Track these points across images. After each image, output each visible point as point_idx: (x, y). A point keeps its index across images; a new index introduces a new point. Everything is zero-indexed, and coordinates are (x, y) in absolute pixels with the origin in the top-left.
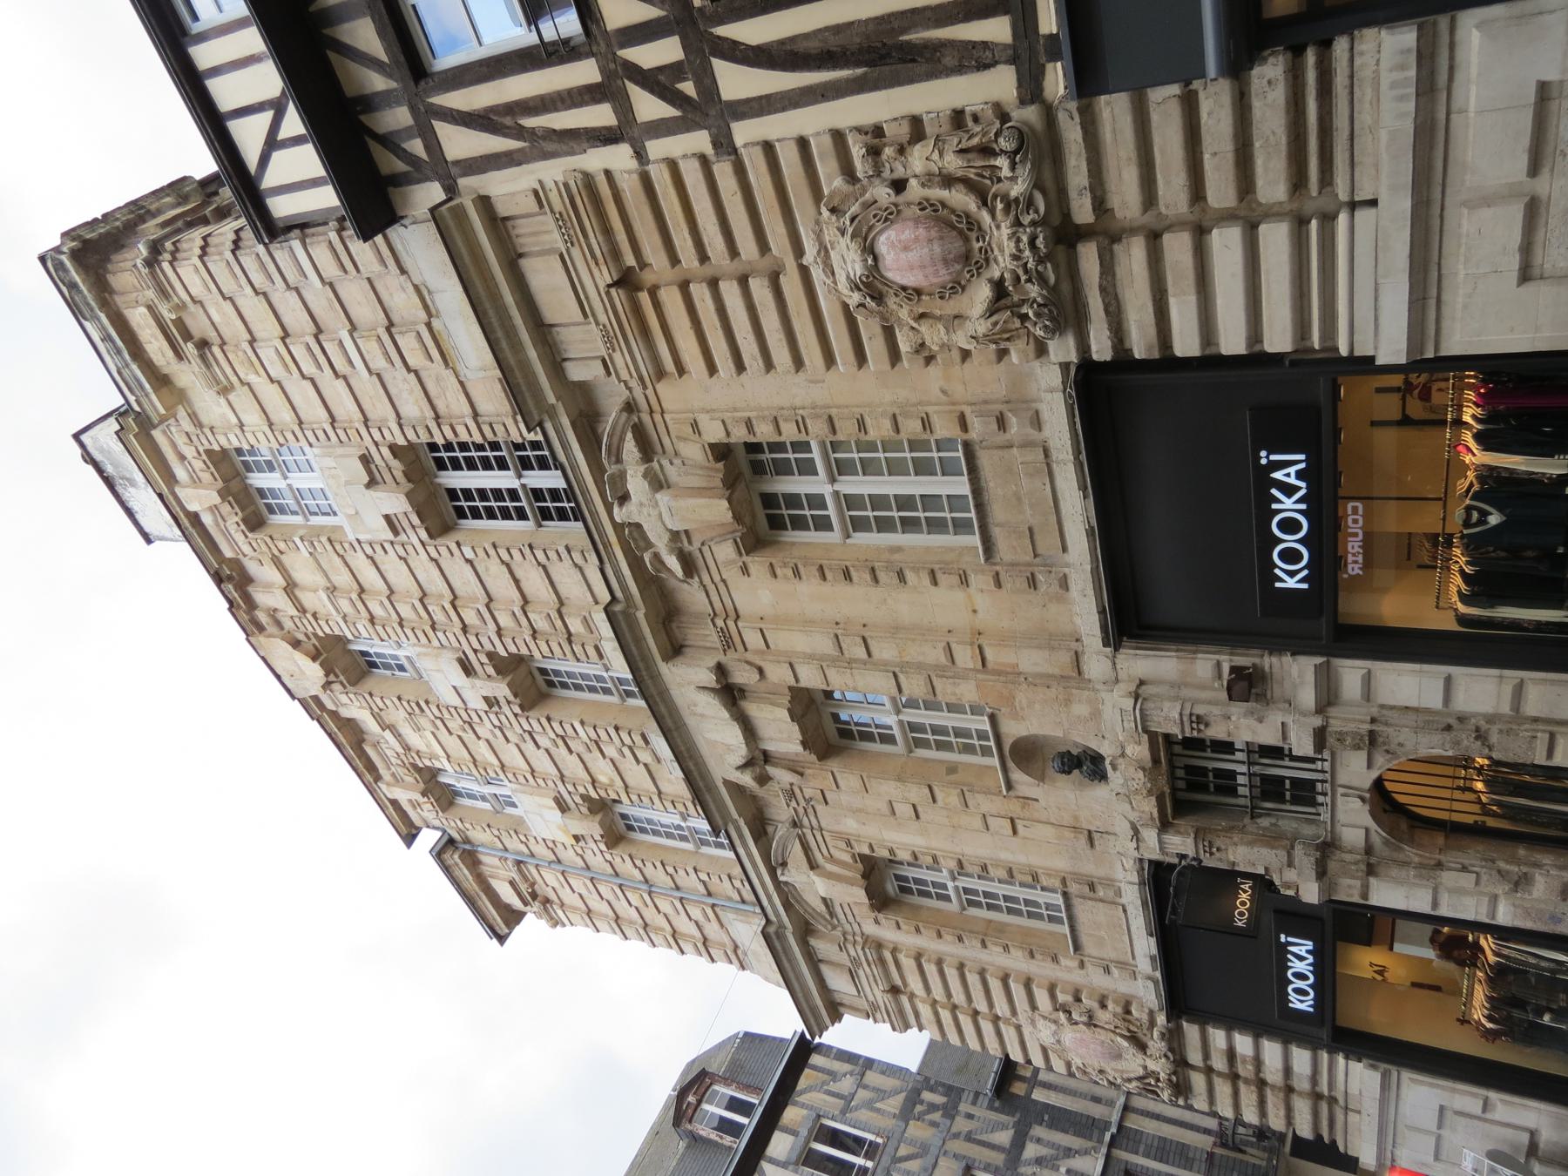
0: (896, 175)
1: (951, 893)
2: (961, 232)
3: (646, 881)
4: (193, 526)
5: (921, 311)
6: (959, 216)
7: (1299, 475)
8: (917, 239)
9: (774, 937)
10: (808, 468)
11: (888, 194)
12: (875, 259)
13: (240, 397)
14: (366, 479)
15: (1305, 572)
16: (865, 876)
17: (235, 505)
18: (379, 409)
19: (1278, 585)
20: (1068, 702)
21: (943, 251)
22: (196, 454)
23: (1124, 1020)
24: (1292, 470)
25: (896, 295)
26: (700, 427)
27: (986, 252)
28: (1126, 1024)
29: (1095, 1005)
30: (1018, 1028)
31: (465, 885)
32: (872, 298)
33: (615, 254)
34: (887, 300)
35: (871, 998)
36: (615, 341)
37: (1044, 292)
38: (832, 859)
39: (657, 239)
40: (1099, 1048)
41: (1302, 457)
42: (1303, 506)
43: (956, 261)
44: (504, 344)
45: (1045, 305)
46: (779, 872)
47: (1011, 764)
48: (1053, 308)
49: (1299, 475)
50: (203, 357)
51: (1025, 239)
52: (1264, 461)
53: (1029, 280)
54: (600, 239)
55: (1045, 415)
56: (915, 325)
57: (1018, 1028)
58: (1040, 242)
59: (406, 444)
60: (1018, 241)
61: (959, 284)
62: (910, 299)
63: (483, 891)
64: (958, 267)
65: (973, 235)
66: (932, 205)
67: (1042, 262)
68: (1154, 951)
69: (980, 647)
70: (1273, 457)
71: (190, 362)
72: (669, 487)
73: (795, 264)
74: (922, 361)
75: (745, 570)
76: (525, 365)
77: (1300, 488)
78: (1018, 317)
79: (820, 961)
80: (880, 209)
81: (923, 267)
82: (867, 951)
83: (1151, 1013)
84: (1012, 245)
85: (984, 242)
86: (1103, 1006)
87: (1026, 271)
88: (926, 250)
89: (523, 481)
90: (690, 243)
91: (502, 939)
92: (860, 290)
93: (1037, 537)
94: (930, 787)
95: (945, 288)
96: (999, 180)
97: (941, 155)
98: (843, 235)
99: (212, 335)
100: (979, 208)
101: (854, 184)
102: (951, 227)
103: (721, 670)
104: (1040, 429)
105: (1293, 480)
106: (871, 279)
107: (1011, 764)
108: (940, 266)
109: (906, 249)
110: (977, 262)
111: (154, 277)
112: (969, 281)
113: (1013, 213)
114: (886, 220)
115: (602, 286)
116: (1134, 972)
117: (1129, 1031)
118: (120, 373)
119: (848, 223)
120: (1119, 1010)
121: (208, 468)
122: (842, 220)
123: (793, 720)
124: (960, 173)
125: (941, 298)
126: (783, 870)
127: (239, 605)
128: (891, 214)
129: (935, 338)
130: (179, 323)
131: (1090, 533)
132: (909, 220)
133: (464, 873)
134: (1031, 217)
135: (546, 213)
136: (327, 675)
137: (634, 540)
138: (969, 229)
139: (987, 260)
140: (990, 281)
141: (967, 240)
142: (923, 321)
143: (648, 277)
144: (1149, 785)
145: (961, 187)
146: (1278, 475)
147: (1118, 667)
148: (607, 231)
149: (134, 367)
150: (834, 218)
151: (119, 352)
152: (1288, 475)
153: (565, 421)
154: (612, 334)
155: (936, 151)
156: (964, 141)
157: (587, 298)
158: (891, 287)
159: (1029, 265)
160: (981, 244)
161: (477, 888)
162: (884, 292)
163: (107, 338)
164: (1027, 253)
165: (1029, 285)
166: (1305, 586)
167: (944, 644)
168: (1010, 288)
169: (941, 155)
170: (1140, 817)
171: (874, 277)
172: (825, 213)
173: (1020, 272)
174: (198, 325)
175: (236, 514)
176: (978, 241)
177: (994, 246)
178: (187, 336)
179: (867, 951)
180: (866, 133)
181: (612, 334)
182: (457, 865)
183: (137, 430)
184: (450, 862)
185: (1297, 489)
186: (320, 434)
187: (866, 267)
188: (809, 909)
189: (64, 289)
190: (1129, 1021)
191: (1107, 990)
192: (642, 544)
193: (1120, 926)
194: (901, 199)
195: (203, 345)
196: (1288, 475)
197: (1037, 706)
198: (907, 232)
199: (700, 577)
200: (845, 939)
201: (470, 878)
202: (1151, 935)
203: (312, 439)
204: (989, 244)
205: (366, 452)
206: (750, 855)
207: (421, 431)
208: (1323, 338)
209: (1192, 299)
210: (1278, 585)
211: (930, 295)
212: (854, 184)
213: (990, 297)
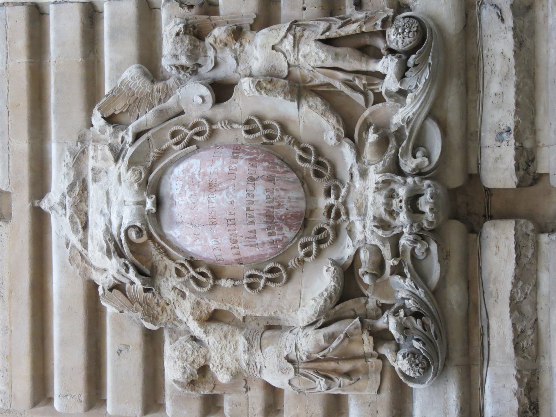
0: (220, 74)
2: (303, 180)
5: (214, 305)
8: (231, 175)
11: (202, 97)
12: (159, 203)
21: (269, 200)
25: (179, 273)
27: (338, 215)
32: (140, 272)
37: (420, 292)
43: (286, 220)
45: (417, 315)
48: (429, 322)
51: (402, 192)
53: (398, 270)
60: (391, 195)
61: (286, 266)
62: (199, 283)
64: (289, 234)
65: (320, 185)
66: (265, 127)
67: (423, 238)
78: (371, 333)
80: (185, 126)
81: (231, 222)
84: (381, 199)
85: (337, 198)
87: (396, 253)
88: (242, 194)
92: (121, 255)
95: (261, 271)
96: (379, 98)
97: (296, 43)
98: (116, 160)
100: (339, 139)
101: (153, 82)
102: (289, 165)
106: (145, 238)
108: (260, 226)
109: (211, 187)
110: (320, 231)
112: (302, 262)
113: (391, 152)
114: (191, 142)
119: (129, 139)
122: (121, 134)
124: (320, 78)
125: (251, 286)
128: (198, 134)
129: (228, 359)
132: (227, 146)
134: (418, 160)
138: (318, 174)
139: (337, 229)
140: (335, 263)
141: (310, 193)
142: (213, 326)
145: (317, 102)
150: (109, 129)
155: (290, 37)
156: (334, 28)
160: (332, 200)
162: (161, 268)
165: (397, 279)
168: (367, 279)
169: (296, 43)
171: (151, 237)
172: (98, 120)
173: (387, 252)
177: (352, 206)
180: (191, 7)
194: (220, 112)
204: (345, 203)
211: (235, 280)
212: (153, 82)
213: (331, 289)
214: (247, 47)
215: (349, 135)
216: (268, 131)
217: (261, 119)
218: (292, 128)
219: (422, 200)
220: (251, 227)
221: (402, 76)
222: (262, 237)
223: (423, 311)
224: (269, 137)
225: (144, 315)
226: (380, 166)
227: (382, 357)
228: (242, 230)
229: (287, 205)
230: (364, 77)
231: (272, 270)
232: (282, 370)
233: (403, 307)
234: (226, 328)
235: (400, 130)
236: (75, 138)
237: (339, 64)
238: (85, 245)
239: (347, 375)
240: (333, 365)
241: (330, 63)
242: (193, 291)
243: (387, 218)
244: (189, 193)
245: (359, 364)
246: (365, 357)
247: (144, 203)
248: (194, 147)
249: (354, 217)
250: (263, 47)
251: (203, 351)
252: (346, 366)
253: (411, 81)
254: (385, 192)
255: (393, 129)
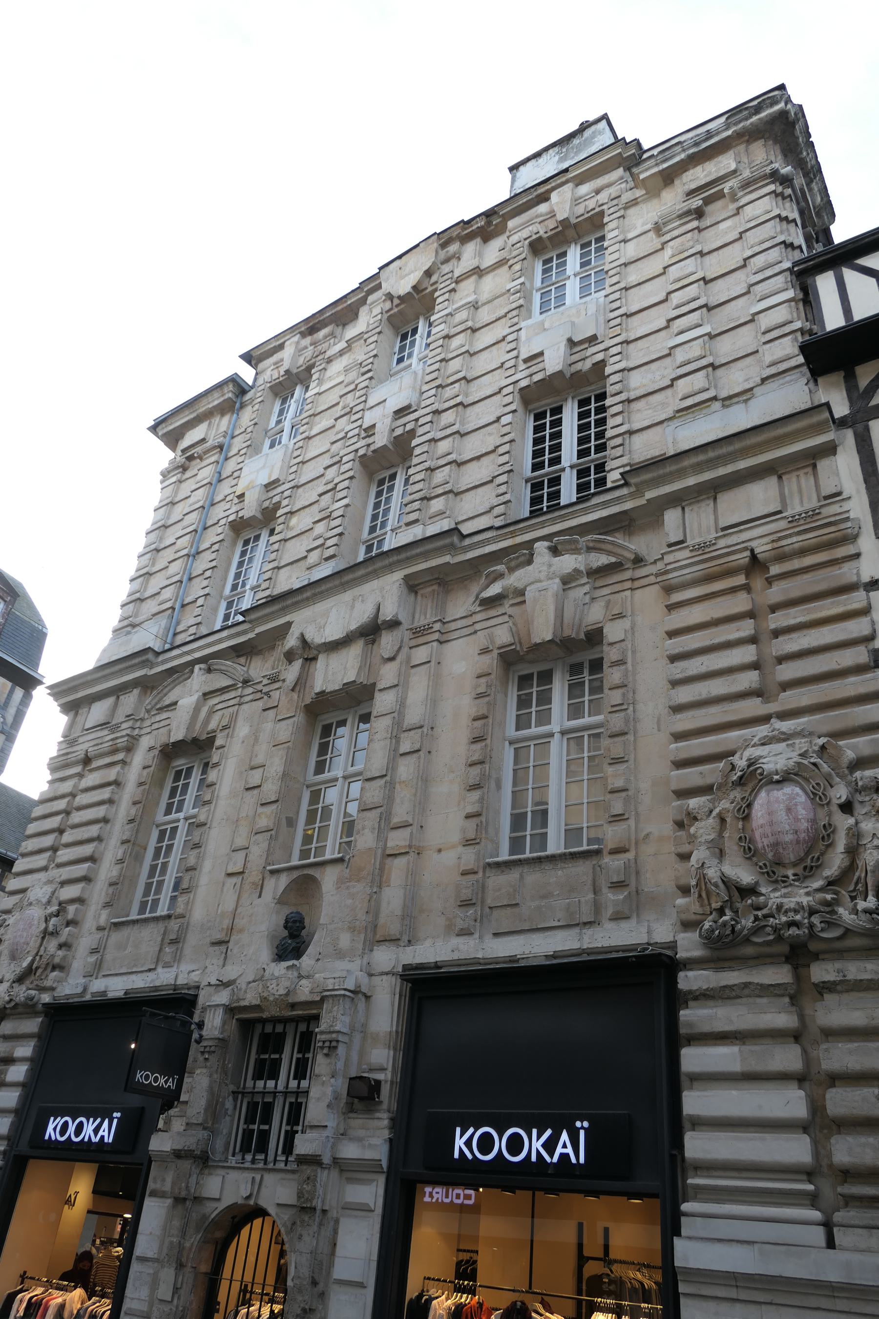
0: (857, 806)
1: (173, 816)
2: (802, 860)
3: (198, 553)
4: (538, 196)
5: (728, 820)
6: (818, 859)
7: (564, 1157)
8: (797, 820)
9: (144, 658)
10: (575, 711)
11: (840, 797)
12: (778, 782)
13: (652, 242)
14: (576, 339)
15: (470, 1156)
16: (195, 740)
17: (553, 232)
18: (637, 354)
19: (458, 1130)
20: (352, 929)
22: (600, 202)
23: (48, 964)
24: (569, 1150)
25: (743, 799)
26: (618, 621)
27: (784, 882)
28: (43, 966)
29: (62, 939)
30: (45, 869)
31: (204, 401)
32: (741, 778)
33: (782, 557)
34: (739, 789)
35: (81, 740)
36: (700, 552)
37: (745, 932)
38: (212, 712)
39: (796, 593)
40: (22, 941)
41: (582, 1160)
42: (534, 1158)
44: (701, 457)
45: (733, 931)
46: (203, 666)
47: (295, 874)
48: (730, 938)
49: (564, 1157)
50: (688, 212)
51: (798, 917)
52: (578, 1124)
53: (756, 918)
54: (796, 546)
55: (624, 924)
56: (714, 813)
57: (45, 869)
58: (793, 931)
59: (606, 374)
60: (796, 911)
61: (753, 856)
63: (198, 416)
65: (799, 870)
66: (828, 835)
67: (775, 931)
68: (111, 995)
69: (407, 853)
70: (582, 1133)
71: (684, 202)
72: (564, 590)
73: (772, 711)
74: (679, 818)
75: (485, 651)
76: (681, 474)
77: (552, 1156)
79: (118, 697)
80: (824, 789)
81: (771, 823)
82: (126, 739)
83: (53, 989)
84: (792, 905)
86: (61, 946)
87: (765, 916)
88: (787, 827)
89: (568, 470)
90: (792, 622)
91: (154, 429)
92: (749, 766)
93: (509, 910)
94: (276, 801)
96: (853, 898)
99: (707, 222)
100: (826, 878)
103: (394, 624)
104: (610, 919)
105: (559, 1150)
106: (760, 778)
107: (295, 874)
108: (772, 839)
109: (789, 810)
111: (760, 178)
115: (753, 544)
116: (91, 976)
117: (37, 968)
118: (769, 98)
119: (812, 760)
120: (57, 960)
121: (588, 212)
122: (815, 755)
123: (344, 685)
126: (204, 669)
127: (466, 229)
129: (701, 831)
130: (720, 195)
131: (513, 959)
133: (216, 400)
134: (819, 925)
135: (819, 501)
136: (399, 297)
137: (518, 557)
138: (805, 868)
139: (776, 882)
143: (758, 583)
144: (271, 999)
145: (847, 863)
146: (565, 1137)
147: (384, 977)
148: (803, 552)
149: (683, 156)
150: (816, 748)
151: (696, 144)
152: (564, 1146)
153: (628, 506)
154: (707, 550)
157: (741, 531)
158: (750, 795)
159: (771, 919)
160: (792, 877)
161: (201, 410)
162: (745, 788)
163: (709, 135)
164: (784, 919)
165: (752, 918)
166: (456, 1155)
167: (411, 822)
168: (749, 901)
170: (241, 989)
171: (761, 780)
173: (765, 911)
174: (716, 210)
175: (546, 232)
176: (795, 875)
177: (790, 889)
178: (708, 201)
179: (126, 739)
181: (707, 550)
182: (223, 395)
183: (625, 156)
184: (226, 390)
185: (551, 1154)
186: (617, 304)
187: (770, 774)
188: (167, 689)
189: (755, 103)
190: (45, 969)
191: (76, 950)
192: (513, 564)
193: (135, 966)
194: (835, 808)
195: (699, 213)
196: (564, 1146)
197: (349, 902)
198: (804, 812)
199: (479, 611)
200: (137, 720)
201: (210, 406)
202: (126, 993)
203: (612, 297)
204: (791, 885)
205: (599, 341)
206: (220, 641)
207: (617, 387)
208: (698, 1187)
209: (736, 1067)
210: (458, 1130)
211: (743, 829)
214: (873, 819)
215: (830, 883)
216: (826, 837)
217: (833, 832)
218: (830, 850)
219: (795, 929)
220: (770, 835)
221: (866, 911)
222: (766, 842)
223: (736, 934)
224: (823, 838)
225: (721, 783)
226: (811, 903)
227: (711, 913)
228: (768, 830)
229: (785, 853)
230: (864, 889)
231: (750, 848)
232: (698, 861)
233: (737, 923)
234: (718, 827)
235: (836, 913)
236: (811, 730)
237: (869, 874)
238: (753, 746)
239: (700, 896)
240: (704, 888)
241: (869, 868)
242: (735, 807)
243: (783, 910)
244: (785, 798)
245: (706, 901)
246: (710, 904)
247: (777, 774)
248: (812, 796)
249: (784, 891)
250: (874, 828)
251: (705, 817)
252: (704, 895)
253: (863, 917)
254: (797, 907)
255: (836, 909)
